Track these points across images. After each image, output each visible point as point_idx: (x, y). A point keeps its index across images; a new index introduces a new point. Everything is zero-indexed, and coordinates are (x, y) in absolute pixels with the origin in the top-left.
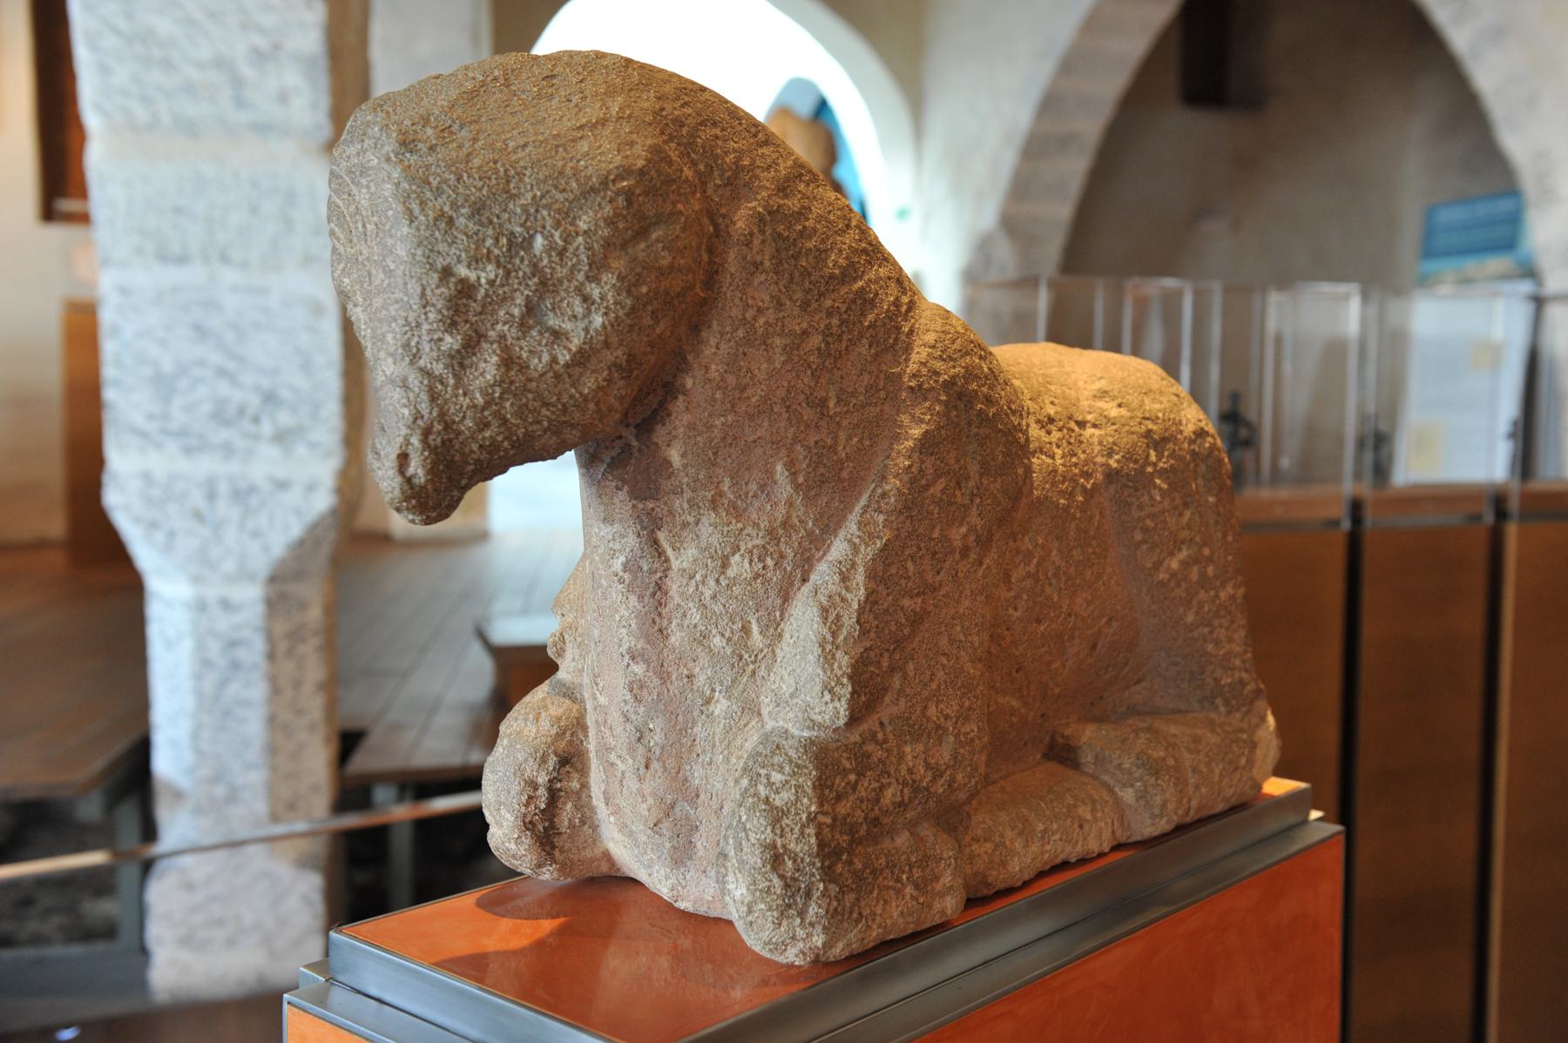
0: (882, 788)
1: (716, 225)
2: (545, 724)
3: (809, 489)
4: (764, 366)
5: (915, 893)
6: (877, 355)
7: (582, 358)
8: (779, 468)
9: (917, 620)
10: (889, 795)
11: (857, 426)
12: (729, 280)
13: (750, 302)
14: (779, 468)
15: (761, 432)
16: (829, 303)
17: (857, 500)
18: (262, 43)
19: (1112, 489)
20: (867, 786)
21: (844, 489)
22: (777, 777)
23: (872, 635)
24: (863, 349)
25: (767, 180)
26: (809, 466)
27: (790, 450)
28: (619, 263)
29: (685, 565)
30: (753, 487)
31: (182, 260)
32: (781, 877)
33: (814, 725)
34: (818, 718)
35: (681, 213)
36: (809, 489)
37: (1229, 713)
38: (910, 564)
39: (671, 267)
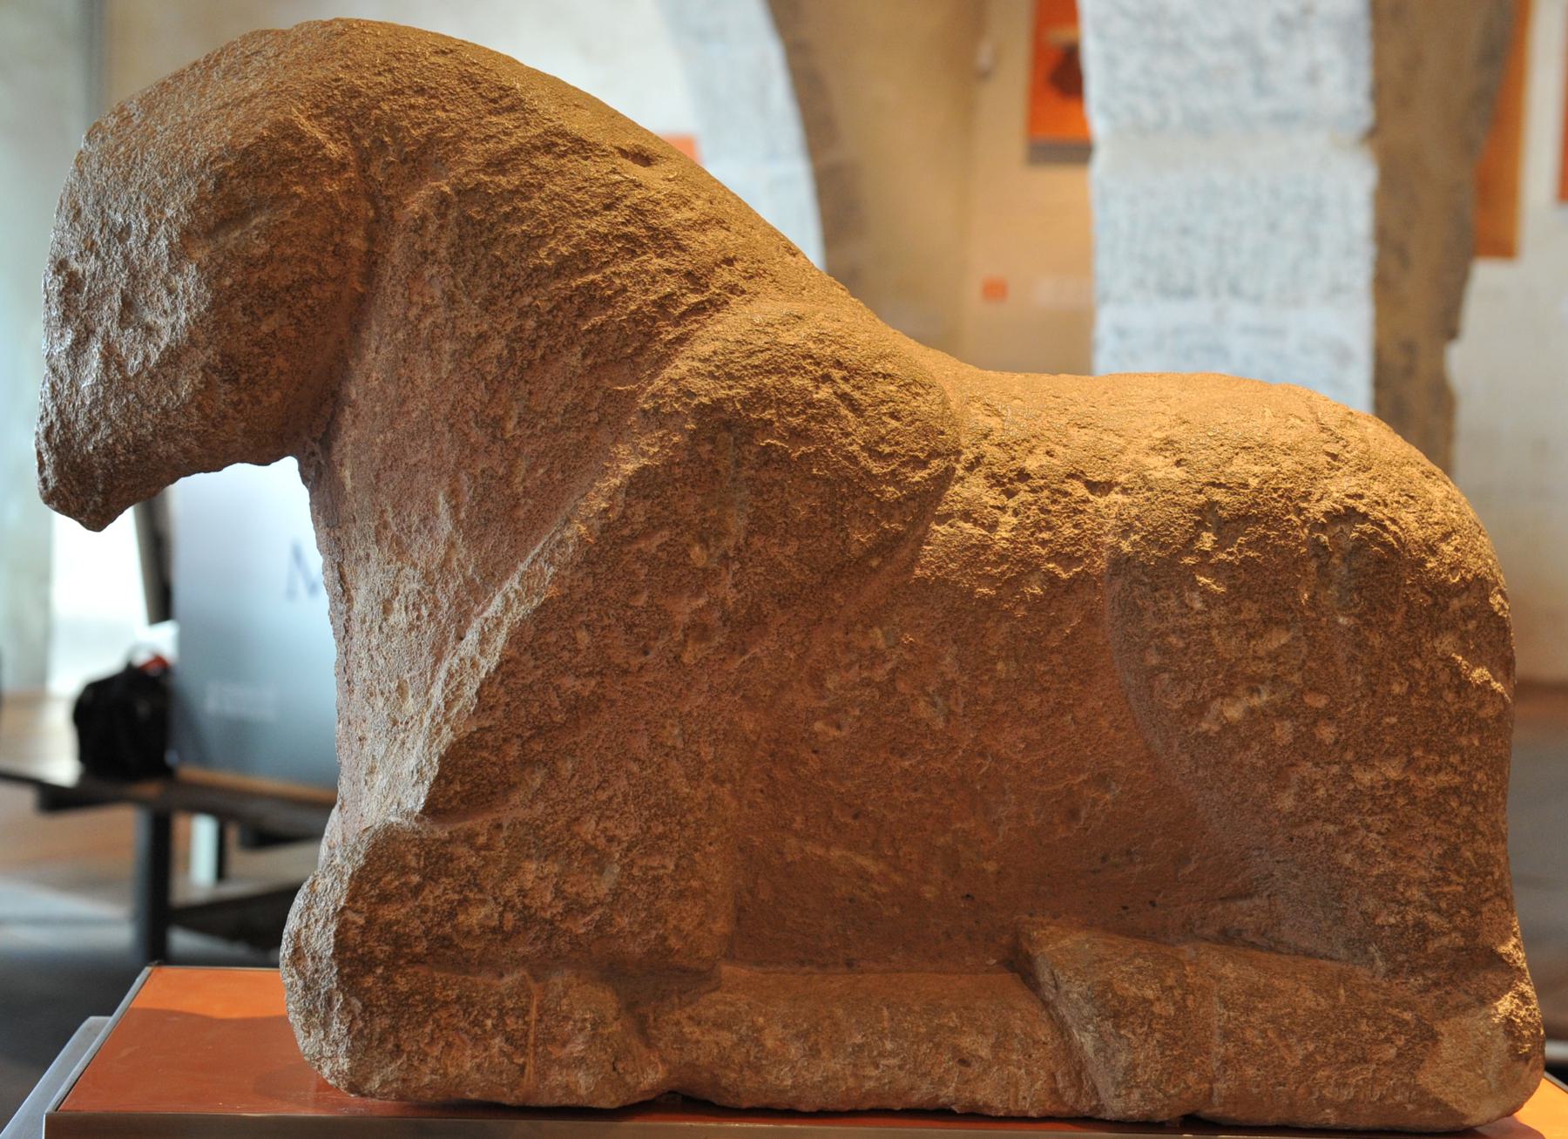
0: (464, 902)
1: (377, 209)
3: (473, 530)
5: (507, 1048)
6: (594, 367)
7: (173, 357)
9: (581, 709)
10: (476, 916)
11: (544, 454)
12: (390, 272)
13: (415, 298)
15: (423, 455)
16: (527, 300)
17: (533, 546)
20: (438, 894)
21: (516, 532)
23: (499, 713)
24: (573, 359)
25: (474, 154)
26: (473, 498)
27: (455, 478)
28: (201, 254)
30: (415, 519)
31: (1187, 293)
32: (301, 974)
35: (296, 195)
36: (472, 527)
37: (1394, 972)
38: (583, 637)
39: (268, 258)
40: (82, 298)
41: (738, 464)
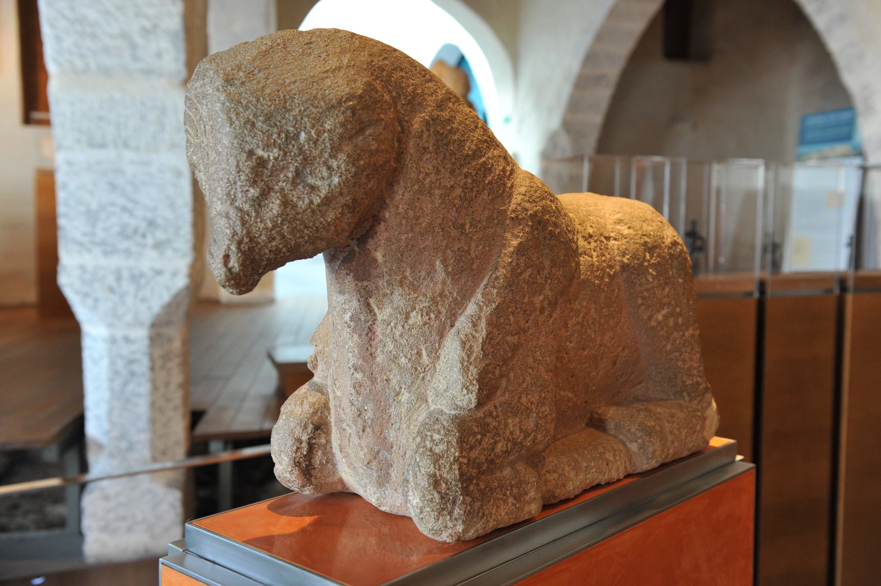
0: (496, 443)
1: (402, 127)
2: (306, 407)
3: (455, 275)
4: (429, 206)
5: (514, 502)
6: (493, 199)
7: (327, 201)
9: (515, 348)
10: (500, 447)
11: (482, 239)
13: (422, 170)
15: (428, 243)
16: (466, 170)
17: (482, 281)
18: (147, 24)
20: (487, 441)
22: (436, 437)
23: (490, 357)
24: (485, 196)
25: (431, 101)
26: (454, 262)
27: (444, 253)
28: (348, 148)
29: (385, 317)
30: (423, 274)
31: (103, 146)
32: (439, 493)
33: (457, 407)
34: (460, 404)
35: (382, 119)
36: (455, 274)
37: (691, 400)
38: (511, 317)
39: (377, 150)
40: (267, 172)
41: (545, 238)
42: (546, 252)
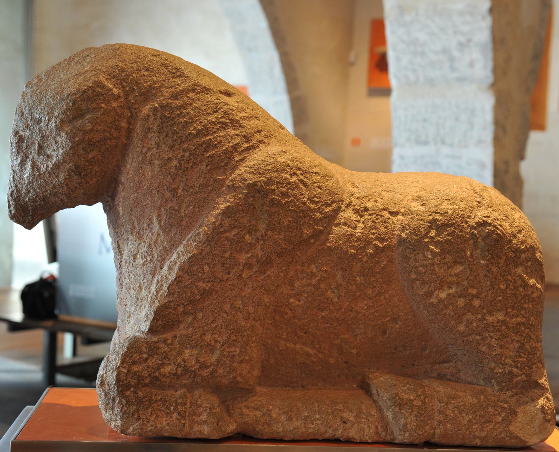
0: (163, 364)
1: (131, 112)
3: (166, 229)
4: (150, 173)
5: (179, 417)
6: (210, 170)
7: (57, 166)
8: (155, 218)
10: (167, 369)
11: (192, 201)
12: (136, 136)
13: (145, 145)
14: (155, 218)
15: (148, 202)
16: (186, 145)
17: (188, 235)
18: (463, 39)
19: (401, 249)
21: (182, 230)
23: (176, 296)
24: (203, 167)
25: (167, 93)
26: (166, 217)
28: (67, 129)
30: (145, 225)
31: (426, 143)
32: (104, 390)
35: (102, 107)
36: (166, 228)
37: (501, 390)
38: (206, 268)
40: (24, 145)
42: (263, 217)
